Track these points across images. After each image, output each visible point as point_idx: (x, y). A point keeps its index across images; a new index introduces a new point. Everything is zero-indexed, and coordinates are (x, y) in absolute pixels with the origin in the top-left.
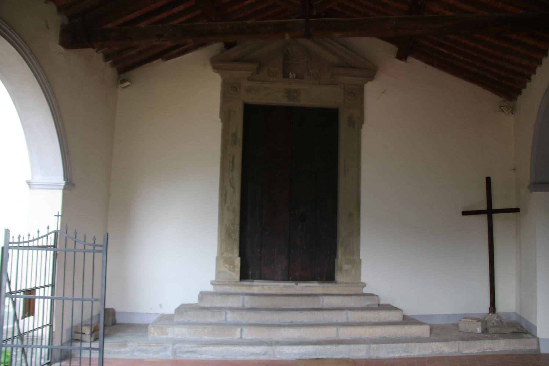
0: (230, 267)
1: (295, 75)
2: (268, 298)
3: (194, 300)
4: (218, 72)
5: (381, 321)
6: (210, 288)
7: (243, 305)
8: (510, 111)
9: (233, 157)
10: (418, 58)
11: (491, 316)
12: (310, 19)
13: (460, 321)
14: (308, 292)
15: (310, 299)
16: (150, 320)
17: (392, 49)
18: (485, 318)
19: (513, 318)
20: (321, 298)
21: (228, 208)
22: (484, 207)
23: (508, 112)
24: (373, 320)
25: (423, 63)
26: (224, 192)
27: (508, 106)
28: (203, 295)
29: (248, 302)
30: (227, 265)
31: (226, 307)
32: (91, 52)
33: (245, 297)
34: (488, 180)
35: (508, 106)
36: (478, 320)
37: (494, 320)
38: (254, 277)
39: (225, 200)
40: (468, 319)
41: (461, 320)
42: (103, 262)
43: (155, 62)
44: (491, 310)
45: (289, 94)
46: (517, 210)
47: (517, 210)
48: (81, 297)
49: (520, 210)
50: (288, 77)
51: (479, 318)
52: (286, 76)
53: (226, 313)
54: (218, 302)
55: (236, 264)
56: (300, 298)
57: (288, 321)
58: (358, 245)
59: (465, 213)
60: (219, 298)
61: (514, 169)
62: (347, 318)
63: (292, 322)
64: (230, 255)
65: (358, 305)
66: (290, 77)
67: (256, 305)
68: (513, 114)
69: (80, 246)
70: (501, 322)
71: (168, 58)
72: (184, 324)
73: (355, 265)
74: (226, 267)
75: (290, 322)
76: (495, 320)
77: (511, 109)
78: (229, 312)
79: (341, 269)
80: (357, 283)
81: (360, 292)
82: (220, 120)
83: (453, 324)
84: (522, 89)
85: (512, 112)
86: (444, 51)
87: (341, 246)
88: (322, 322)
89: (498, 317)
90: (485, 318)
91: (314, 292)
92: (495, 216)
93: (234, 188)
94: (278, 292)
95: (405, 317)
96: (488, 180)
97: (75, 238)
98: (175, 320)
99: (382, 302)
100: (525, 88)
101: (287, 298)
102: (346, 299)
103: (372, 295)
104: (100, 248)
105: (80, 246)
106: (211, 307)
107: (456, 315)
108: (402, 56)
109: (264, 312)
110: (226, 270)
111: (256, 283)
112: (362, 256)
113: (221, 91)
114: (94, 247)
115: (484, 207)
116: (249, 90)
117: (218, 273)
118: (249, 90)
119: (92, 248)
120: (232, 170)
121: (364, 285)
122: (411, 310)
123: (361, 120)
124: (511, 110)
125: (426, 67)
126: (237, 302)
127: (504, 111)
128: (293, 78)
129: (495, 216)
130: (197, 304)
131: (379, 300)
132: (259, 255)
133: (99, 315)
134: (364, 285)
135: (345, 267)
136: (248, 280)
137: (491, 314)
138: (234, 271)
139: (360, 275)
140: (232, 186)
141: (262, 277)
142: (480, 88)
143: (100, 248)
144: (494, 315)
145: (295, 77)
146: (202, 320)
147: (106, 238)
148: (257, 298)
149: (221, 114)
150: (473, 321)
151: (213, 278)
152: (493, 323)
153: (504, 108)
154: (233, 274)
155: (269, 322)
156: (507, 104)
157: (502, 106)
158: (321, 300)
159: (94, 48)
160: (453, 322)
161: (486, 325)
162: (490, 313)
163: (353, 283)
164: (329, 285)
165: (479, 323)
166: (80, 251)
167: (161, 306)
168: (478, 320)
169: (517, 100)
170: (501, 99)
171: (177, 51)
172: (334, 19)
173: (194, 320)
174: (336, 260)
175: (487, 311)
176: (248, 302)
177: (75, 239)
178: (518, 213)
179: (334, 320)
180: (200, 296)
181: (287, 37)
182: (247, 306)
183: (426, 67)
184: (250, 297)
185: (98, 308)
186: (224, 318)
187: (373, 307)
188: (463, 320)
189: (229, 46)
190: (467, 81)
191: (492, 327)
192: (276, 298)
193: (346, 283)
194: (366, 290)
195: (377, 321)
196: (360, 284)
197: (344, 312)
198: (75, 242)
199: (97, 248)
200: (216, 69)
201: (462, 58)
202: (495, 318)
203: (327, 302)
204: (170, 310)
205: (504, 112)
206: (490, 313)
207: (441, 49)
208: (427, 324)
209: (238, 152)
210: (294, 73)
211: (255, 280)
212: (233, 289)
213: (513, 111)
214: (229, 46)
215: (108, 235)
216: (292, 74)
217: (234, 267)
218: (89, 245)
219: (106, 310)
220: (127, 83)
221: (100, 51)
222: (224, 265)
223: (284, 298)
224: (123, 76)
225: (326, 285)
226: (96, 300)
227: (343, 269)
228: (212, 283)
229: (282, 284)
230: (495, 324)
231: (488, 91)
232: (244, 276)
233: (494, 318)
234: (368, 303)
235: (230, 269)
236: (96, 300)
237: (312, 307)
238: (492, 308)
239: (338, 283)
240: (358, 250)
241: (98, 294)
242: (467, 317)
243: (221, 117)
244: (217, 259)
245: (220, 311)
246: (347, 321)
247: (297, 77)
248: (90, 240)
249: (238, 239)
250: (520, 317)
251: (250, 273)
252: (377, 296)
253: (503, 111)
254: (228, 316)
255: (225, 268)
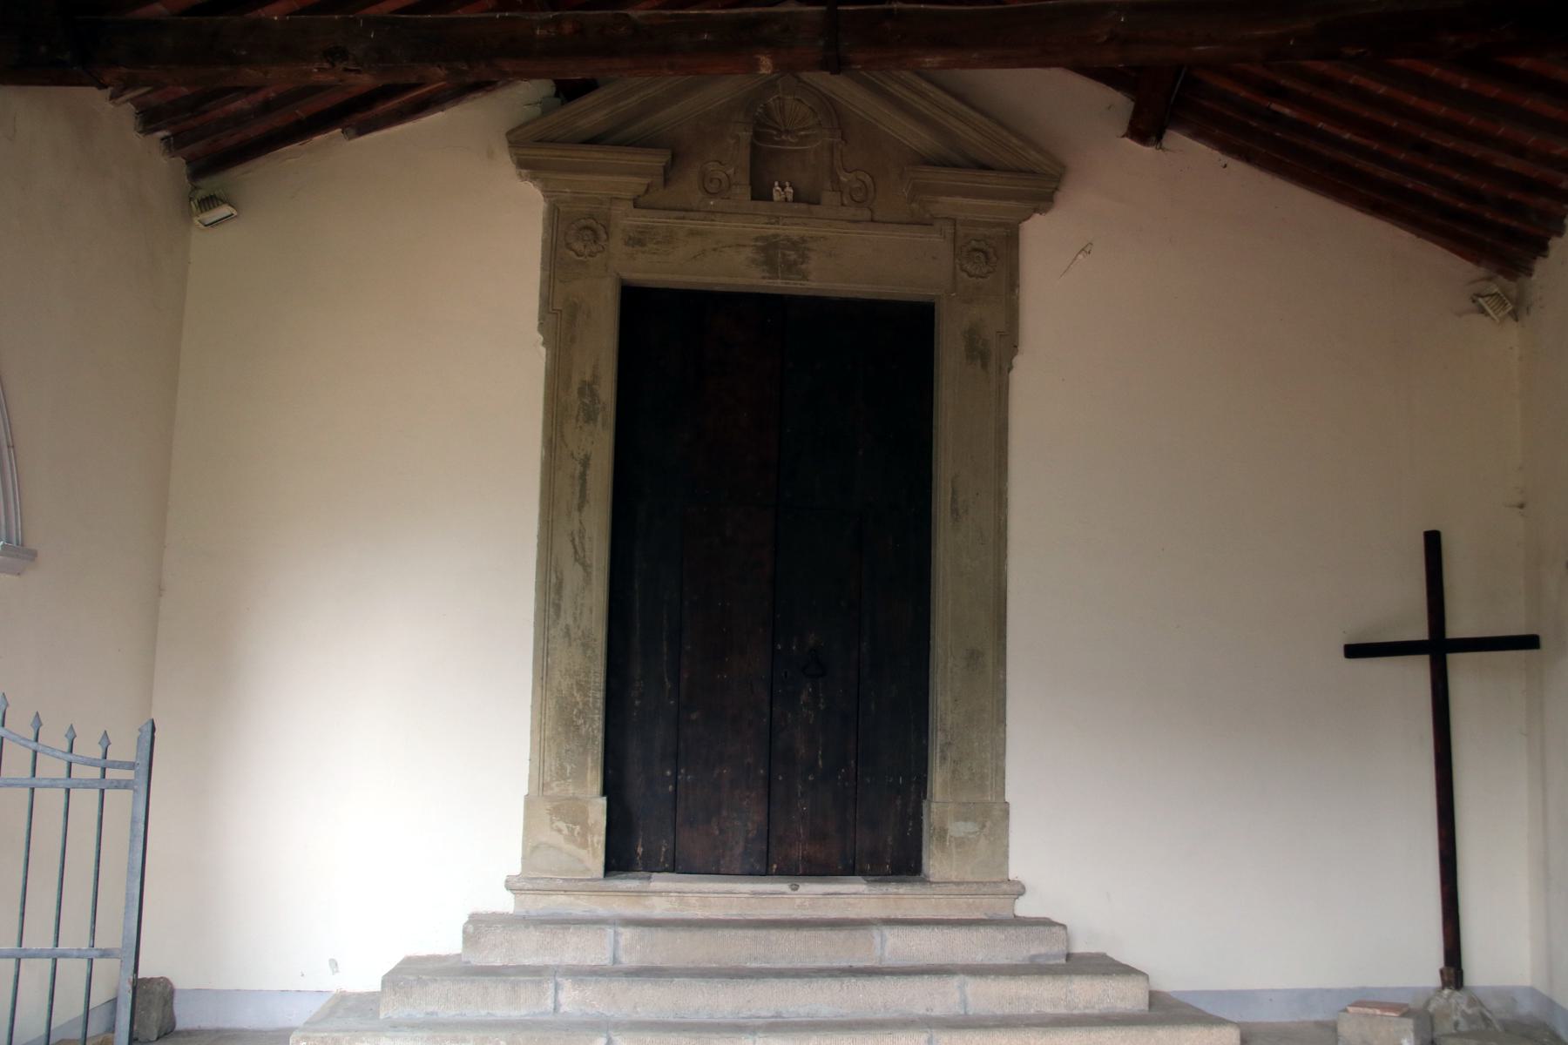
0: (571, 831)
1: (789, 190)
2: (700, 935)
3: (449, 943)
4: (533, 179)
5: (1076, 1012)
6: (505, 903)
7: (615, 960)
8: (1509, 313)
9: (585, 463)
10: (1198, 135)
11: (1449, 996)
12: (839, 8)
13: (1342, 1014)
14: (833, 914)
15: (839, 936)
16: (294, 1015)
17: (1119, 103)
18: (1428, 1003)
19: (1526, 1008)
20: (875, 932)
21: (567, 633)
22: (1419, 631)
23: (1500, 315)
24: (1049, 1010)
25: (1217, 154)
26: (554, 580)
27: (1502, 295)
28: (479, 926)
29: (633, 948)
30: (562, 825)
31: (558, 966)
32: (93, 98)
33: (621, 930)
34: (1433, 541)
35: (1502, 295)
36: (1406, 1012)
37: (1459, 1014)
38: (651, 866)
39: (558, 607)
40: (1370, 1007)
41: (1346, 1010)
42: (134, 821)
43: (318, 139)
44: (1446, 978)
45: (770, 252)
46: (1529, 642)
47: (1529, 642)
48: (49, 945)
49: (1543, 642)
50: (769, 198)
51: (1406, 1005)
52: (760, 193)
53: (557, 988)
54: (530, 950)
55: (590, 822)
56: (805, 934)
57: (763, 1013)
58: (1000, 755)
59: (1353, 651)
60: (535, 935)
61: (1521, 506)
62: (964, 1002)
63: (779, 1015)
64: (571, 790)
65: (1001, 958)
66: (776, 196)
67: (658, 960)
68: (1517, 320)
69: (51, 768)
70: (1485, 1018)
71: (364, 129)
72: (415, 1026)
73: (988, 824)
74: (560, 831)
75: (772, 1017)
76: (1464, 1015)
77: (1509, 304)
78: (567, 984)
79: (943, 832)
80: (994, 882)
81: (1005, 914)
82: (540, 338)
83: (1320, 1025)
84: (1549, 239)
85: (1515, 315)
86: (1287, 111)
87: (944, 758)
88: (880, 1016)
89: (1474, 1001)
90: (1428, 1003)
91: (851, 914)
92: (1458, 663)
93: (586, 567)
94: (733, 913)
95: (1155, 998)
96: (1433, 541)
97: (37, 740)
98: (382, 1016)
99: (1080, 948)
100: (1560, 234)
101: (762, 934)
102: (959, 936)
103: (1047, 923)
104: (127, 775)
105: (51, 768)
106: (505, 967)
107: (1329, 991)
108: (1146, 129)
109: (687, 980)
110: (559, 840)
111: (660, 882)
112: (1009, 796)
113: (544, 241)
114: (104, 770)
115: (1419, 631)
116: (637, 240)
117: (531, 850)
118: (637, 240)
119: (96, 773)
120: (580, 508)
121: (1019, 890)
122: (1174, 978)
123: (1010, 341)
124: (1510, 307)
125: (1225, 166)
126: (591, 949)
127: (1490, 311)
128: (786, 199)
129: (1458, 663)
130: (459, 955)
131: (1068, 940)
132: (671, 788)
133: (114, 1002)
134: (1019, 890)
135: (957, 829)
136: (630, 874)
137: (1446, 992)
138: (584, 845)
139: (1006, 856)
140: (580, 559)
141: (677, 865)
142: (1406, 235)
143: (127, 775)
144: (1457, 993)
145: (790, 197)
146: (475, 1011)
147: (148, 738)
148: (660, 934)
149: (542, 318)
150: (1387, 1014)
151: (516, 868)
152: (1456, 1024)
153: (1487, 302)
154: (582, 853)
155: (703, 1017)
156: (1496, 290)
157: (1479, 296)
158: (878, 940)
159: (102, 86)
160: (1319, 1017)
161: (1433, 1029)
162: (1443, 988)
163: (984, 884)
164: (904, 889)
165: (1409, 1024)
166: (53, 784)
167: (334, 964)
168: (1406, 1012)
169: (1531, 275)
170: (1481, 272)
171: (394, 103)
172: (922, 6)
173: (448, 1012)
174: (925, 804)
175: (1434, 980)
176: (633, 948)
177: (34, 745)
178: (1535, 651)
179: (919, 1010)
180: (471, 929)
181: (766, 66)
182: (628, 961)
183: (1225, 166)
184: (639, 930)
185: (110, 980)
186: (550, 1004)
187: (1052, 962)
188: (1351, 1009)
189: (569, 91)
190: (1362, 211)
191: (1452, 1035)
192: (727, 933)
193: (958, 884)
194: (1025, 908)
195: (1062, 1010)
196: (1005, 887)
197: (955, 981)
198: (35, 753)
199: (112, 774)
200: (529, 166)
201: (1347, 136)
202: (1464, 1007)
203: (897, 946)
204: (365, 978)
205: (1487, 315)
206: (1443, 988)
207: (1274, 107)
208: (1231, 1022)
209: (599, 445)
210: (787, 184)
211: (655, 875)
212: (581, 905)
213: (1517, 309)
214: (569, 91)
215: (153, 729)
216: (783, 188)
217: (586, 829)
218: (85, 764)
219: (139, 986)
220: (225, 210)
221: (129, 95)
222: (552, 822)
223: (751, 933)
224: (209, 185)
225: (892, 888)
226: (105, 954)
227: (948, 837)
228: (510, 885)
229: (745, 887)
230: (1463, 1027)
231: (1431, 244)
232: (619, 860)
233: (1458, 1004)
234: (1033, 952)
235: (571, 838)
236: (105, 954)
237: (844, 964)
238: (1452, 971)
239: (932, 883)
240: (1000, 772)
241: (112, 933)
242: (1366, 1001)
243: (542, 327)
244: (529, 802)
245: (537, 978)
246: (962, 1012)
247: (797, 198)
248: (88, 747)
249: (600, 736)
250: (1550, 1004)
251: (640, 850)
252: (1064, 926)
253: (1483, 311)
254: (563, 997)
255: (554, 835)
